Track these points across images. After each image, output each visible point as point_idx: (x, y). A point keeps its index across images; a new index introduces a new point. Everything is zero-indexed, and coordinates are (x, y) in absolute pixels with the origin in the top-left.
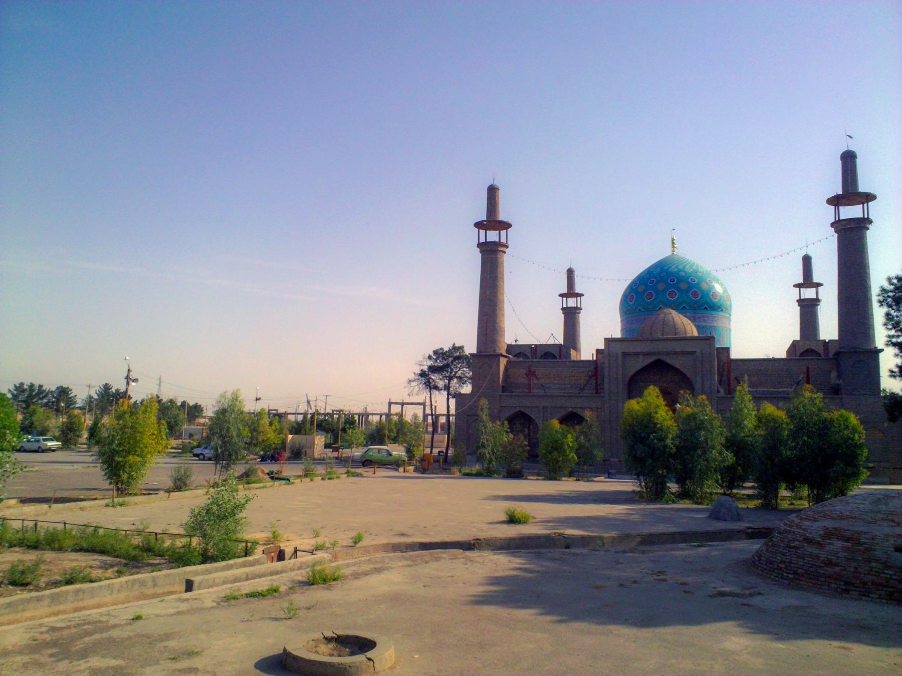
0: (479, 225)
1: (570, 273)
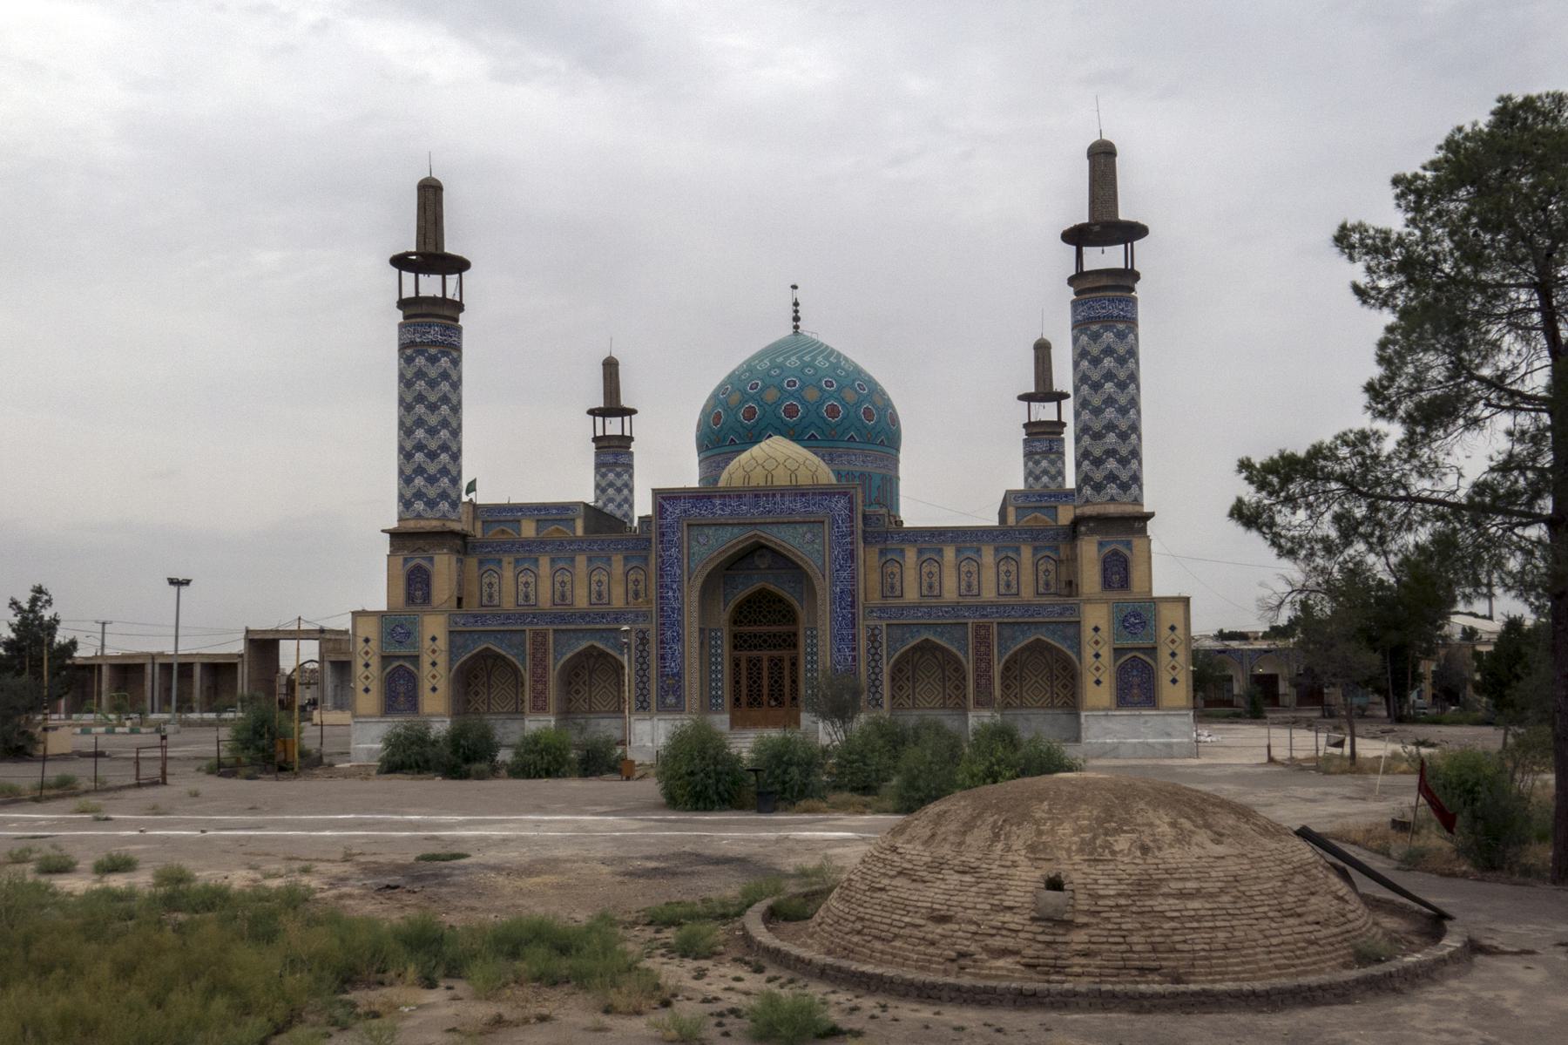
0: (400, 262)
1: (611, 368)
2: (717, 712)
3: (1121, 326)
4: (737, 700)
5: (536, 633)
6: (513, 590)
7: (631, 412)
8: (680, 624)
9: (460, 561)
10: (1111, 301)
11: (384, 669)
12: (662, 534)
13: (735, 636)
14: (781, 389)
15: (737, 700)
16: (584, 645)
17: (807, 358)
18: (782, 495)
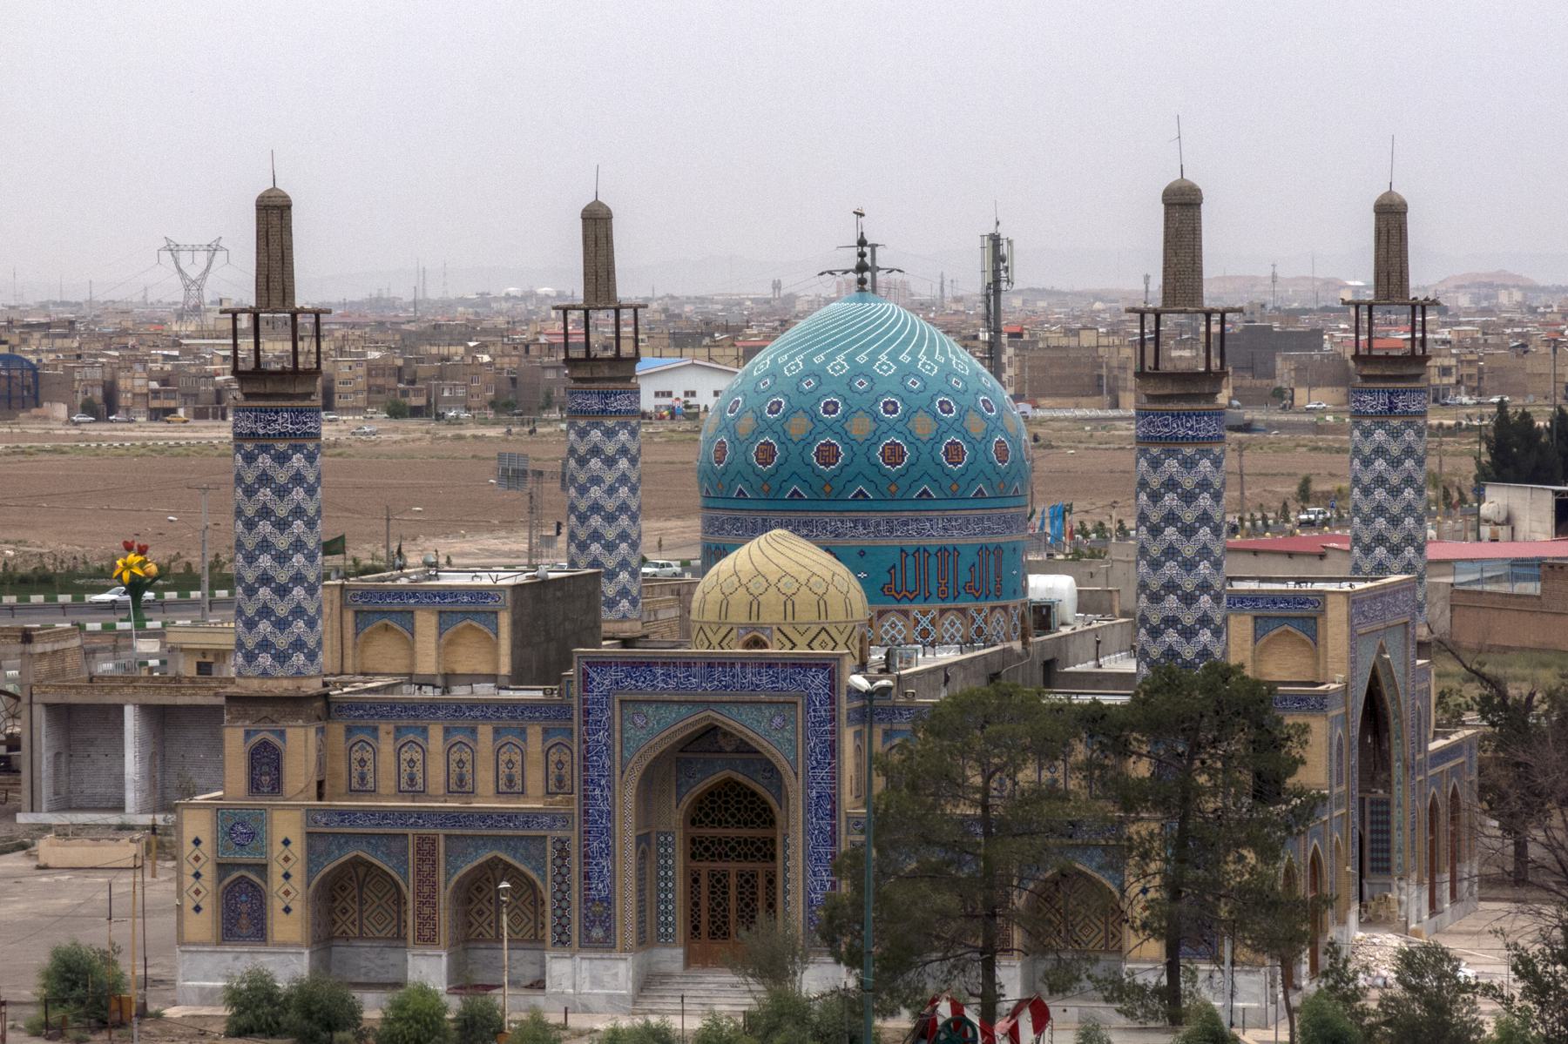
2: (666, 945)
4: (696, 928)
5: (422, 839)
6: (393, 768)
8: (610, 832)
9: (320, 731)
10: (1177, 416)
11: (220, 881)
12: (587, 713)
13: (693, 841)
14: (814, 417)
15: (696, 928)
16: (486, 855)
17: (862, 358)
18: (744, 665)
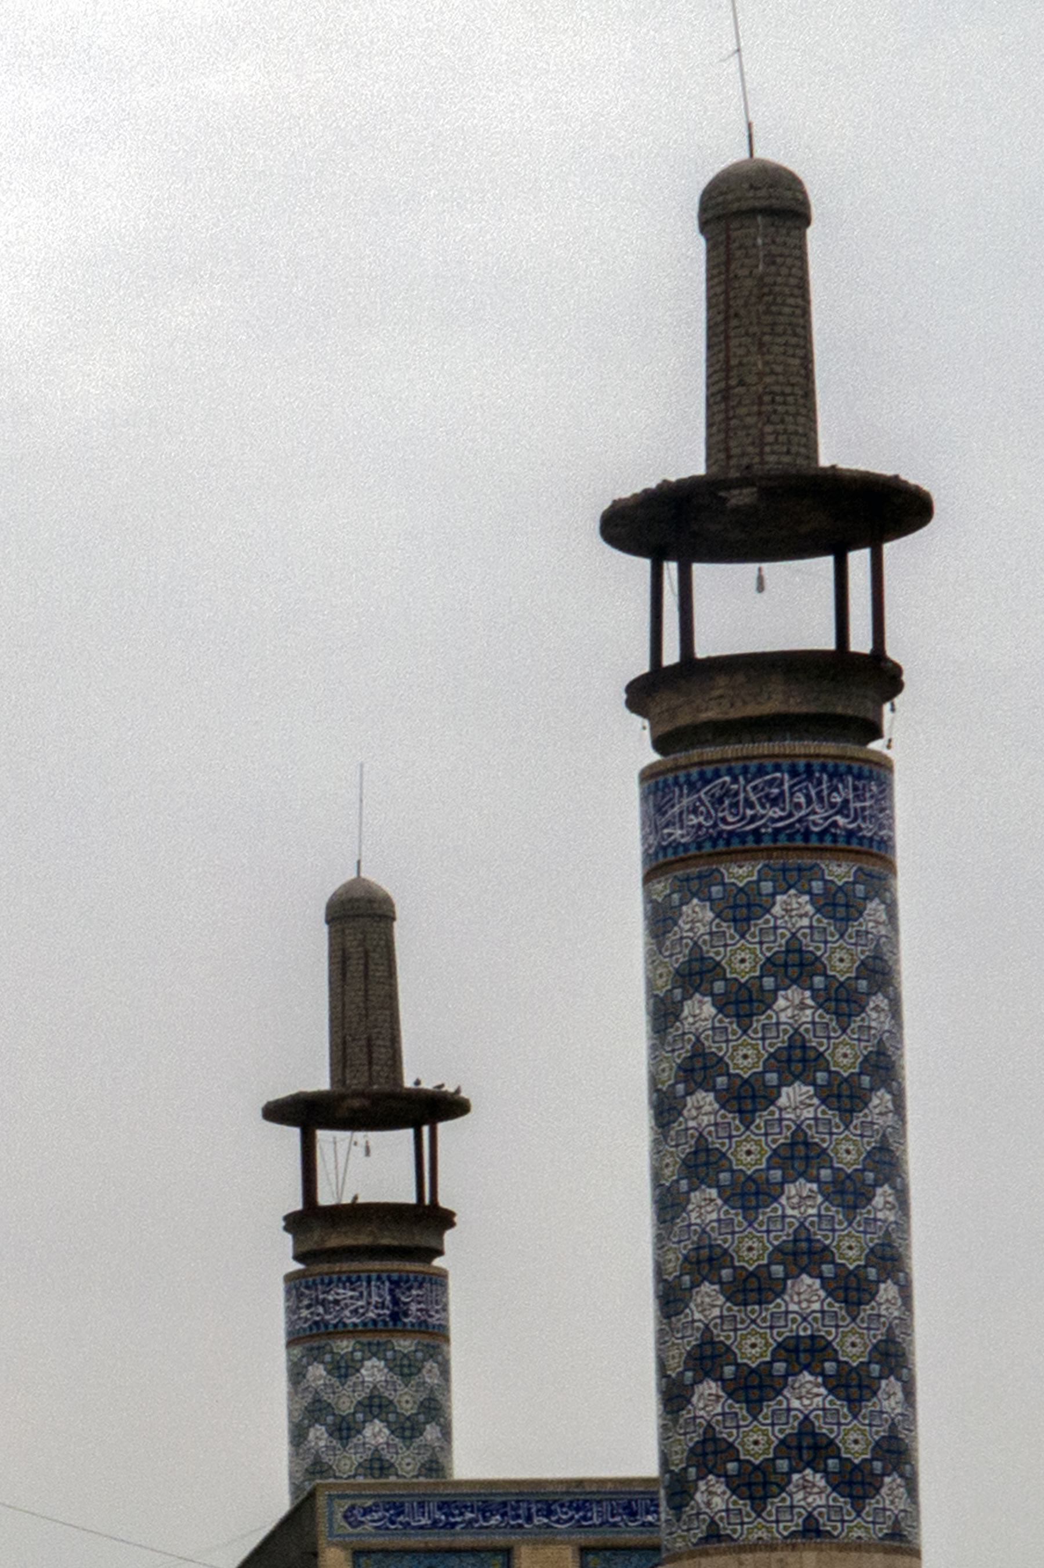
3: (839, 872)
7: (445, 1106)
10: (804, 772)
